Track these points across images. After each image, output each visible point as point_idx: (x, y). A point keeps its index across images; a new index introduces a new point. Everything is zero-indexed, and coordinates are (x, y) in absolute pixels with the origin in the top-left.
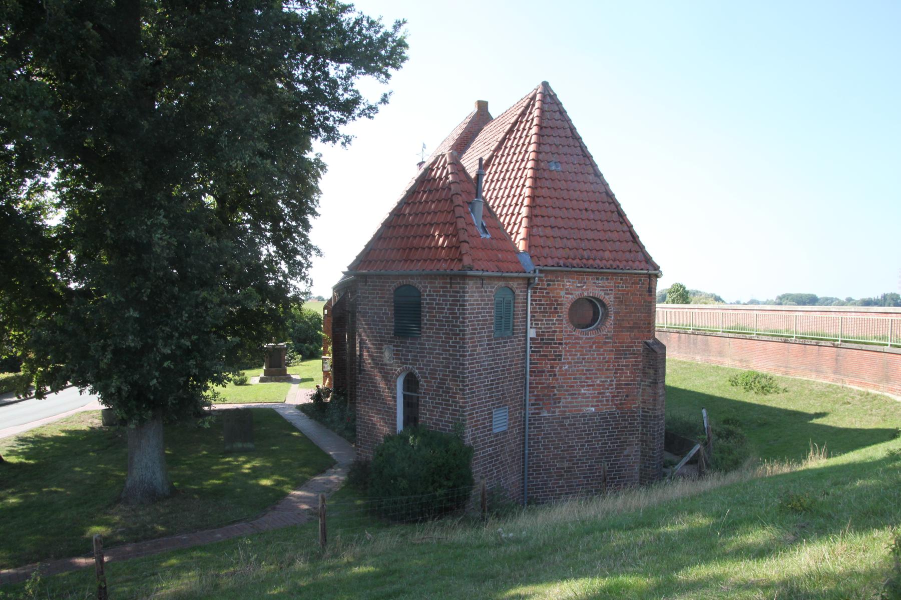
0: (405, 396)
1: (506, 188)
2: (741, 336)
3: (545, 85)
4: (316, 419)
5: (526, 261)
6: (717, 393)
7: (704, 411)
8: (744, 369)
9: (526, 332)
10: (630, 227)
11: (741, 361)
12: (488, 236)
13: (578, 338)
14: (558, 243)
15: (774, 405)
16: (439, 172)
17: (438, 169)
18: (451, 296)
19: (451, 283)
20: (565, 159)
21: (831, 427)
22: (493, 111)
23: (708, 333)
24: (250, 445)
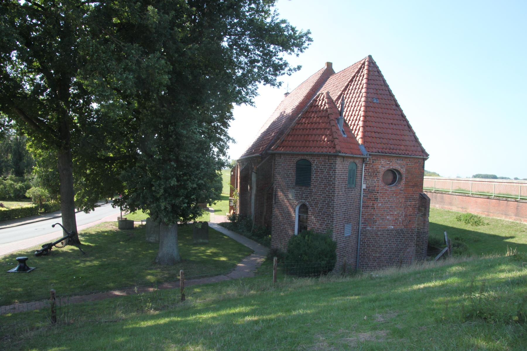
1: (350, 111)
2: (463, 194)
3: (370, 57)
4: (232, 230)
5: (363, 149)
6: (450, 225)
7: (445, 233)
8: (464, 213)
9: (361, 186)
10: (414, 133)
11: (462, 208)
12: (346, 136)
13: (386, 190)
14: (378, 141)
15: (482, 232)
16: (320, 102)
17: (320, 100)
18: (328, 166)
19: (328, 159)
20: (381, 97)
21: (515, 243)
22: (336, 68)
23: (444, 192)
24: (206, 241)
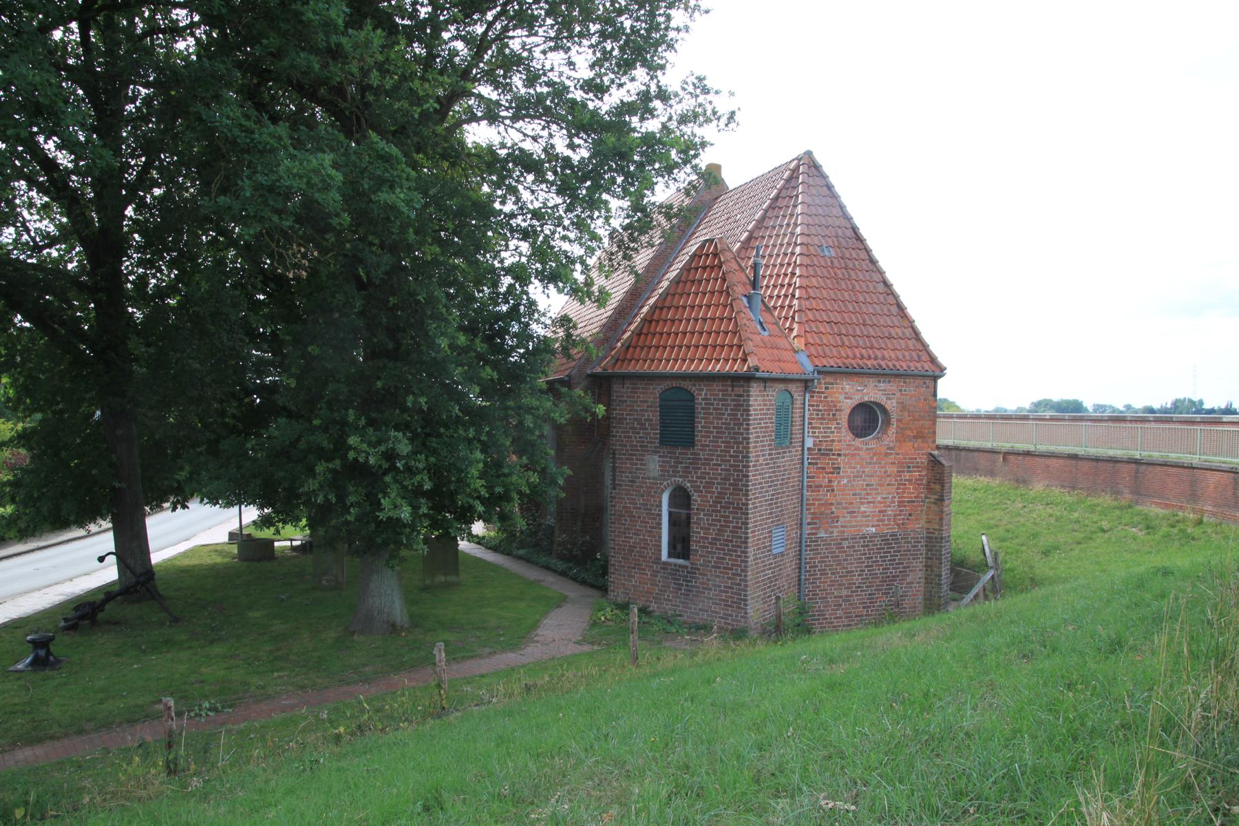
0: (670, 514)
10: (912, 322)
13: (857, 449)
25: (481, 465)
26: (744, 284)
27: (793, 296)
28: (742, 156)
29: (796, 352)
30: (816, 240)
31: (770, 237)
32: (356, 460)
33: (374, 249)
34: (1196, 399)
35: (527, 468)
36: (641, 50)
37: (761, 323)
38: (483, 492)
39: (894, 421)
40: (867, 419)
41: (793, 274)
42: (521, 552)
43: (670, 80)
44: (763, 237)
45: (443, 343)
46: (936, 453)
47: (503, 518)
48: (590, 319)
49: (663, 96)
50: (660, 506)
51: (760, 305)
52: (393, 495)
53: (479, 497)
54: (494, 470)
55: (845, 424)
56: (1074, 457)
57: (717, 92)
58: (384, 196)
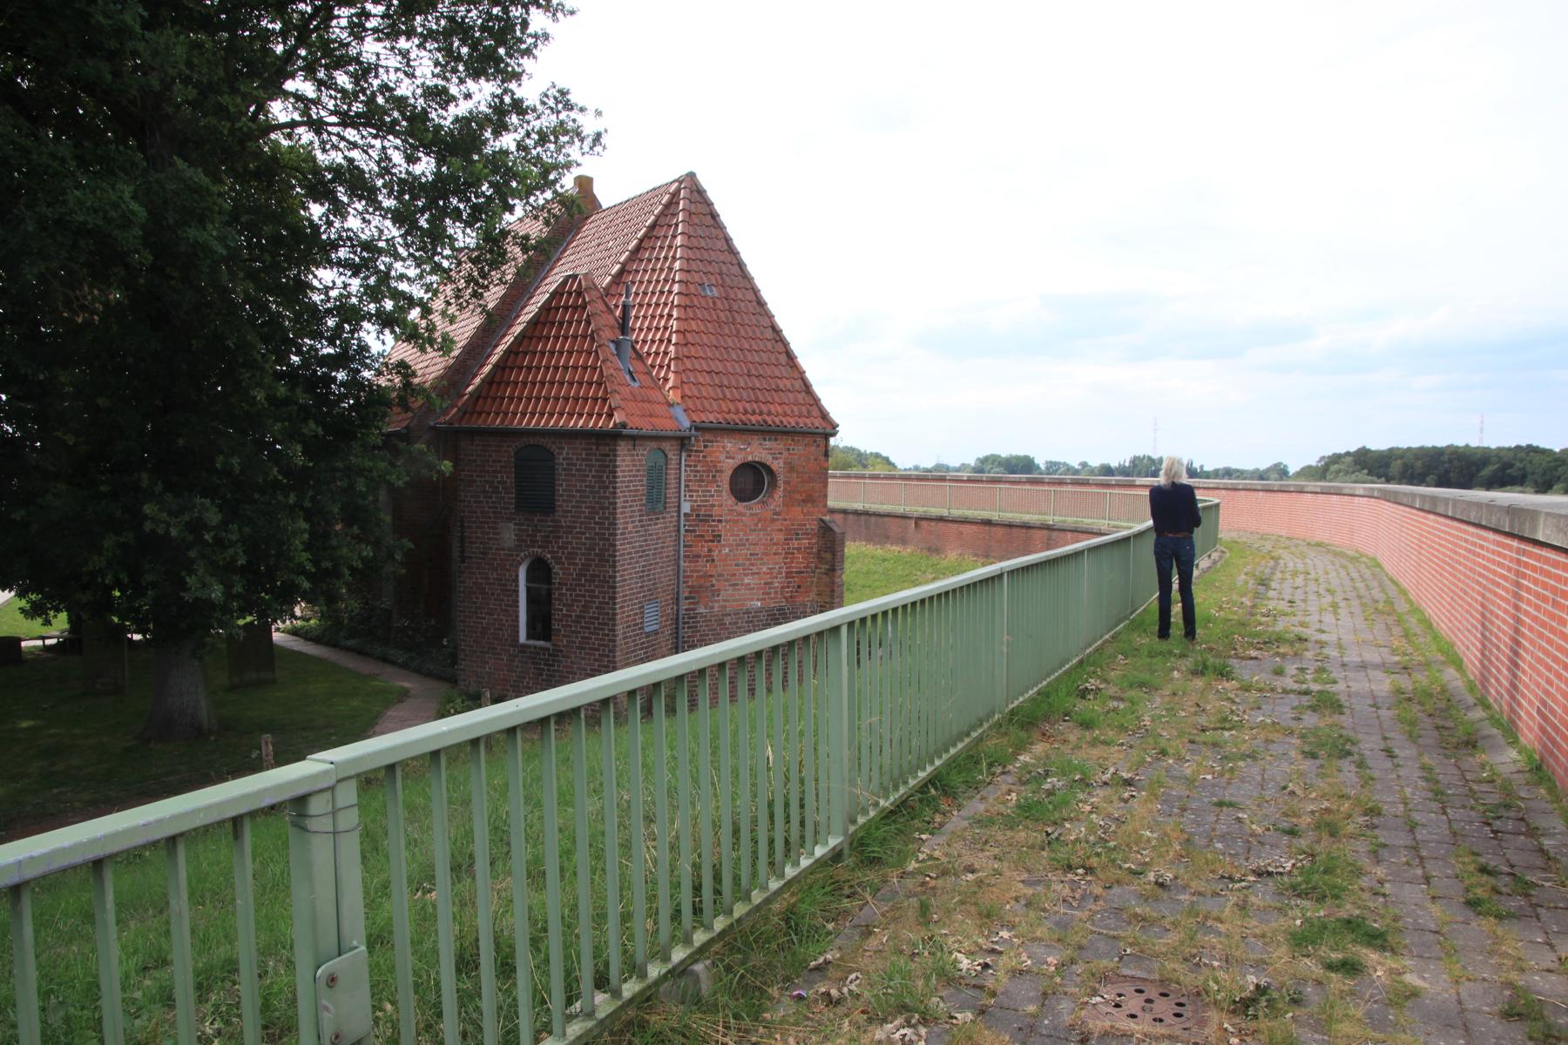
0: (529, 590)
10: (802, 373)
25: (306, 536)
26: (612, 327)
27: (669, 341)
28: (620, 174)
29: (670, 405)
30: (697, 277)
31: (645, 271)
32: (153, 531)
33: (173, 283)
34: (1155, 457)
35: (358, 539)
36: (491, 48)
37: (630, 373)
38: (309, 566)
39: (781, 483)
40: (752, 481)
41: (670, 316)
42: (350, 643)
43: (529, 91)
44: (637, 271)
45: (260, 396)
46: (827, 518)
47: (331, 599)
48: (429, 366)
49: (518, 107)
50: (516, 580)
51: (630, 352)
52: (201, 572)
53: (304, 572)
54: (319, 542)
55: (726, 486)
56: (988, 523)
57: (582, 110)
58: (192, 233)
